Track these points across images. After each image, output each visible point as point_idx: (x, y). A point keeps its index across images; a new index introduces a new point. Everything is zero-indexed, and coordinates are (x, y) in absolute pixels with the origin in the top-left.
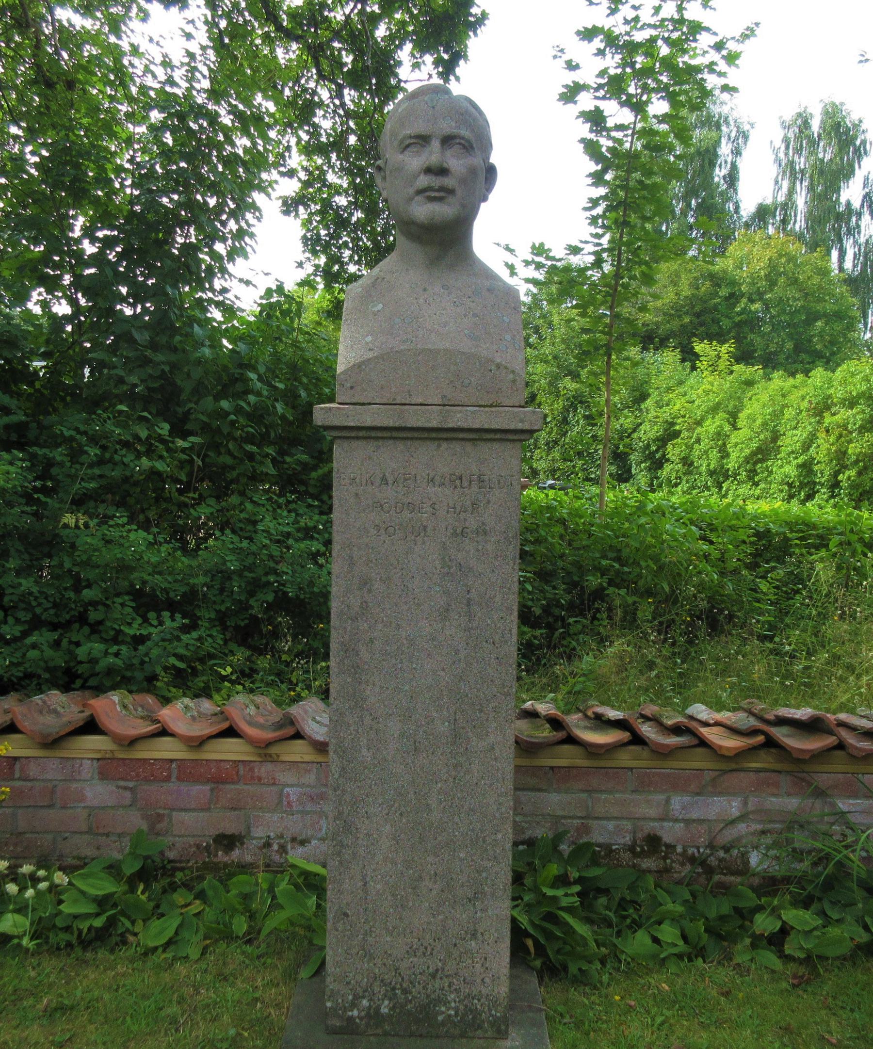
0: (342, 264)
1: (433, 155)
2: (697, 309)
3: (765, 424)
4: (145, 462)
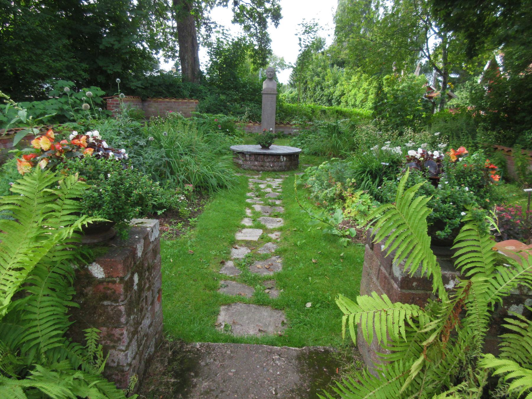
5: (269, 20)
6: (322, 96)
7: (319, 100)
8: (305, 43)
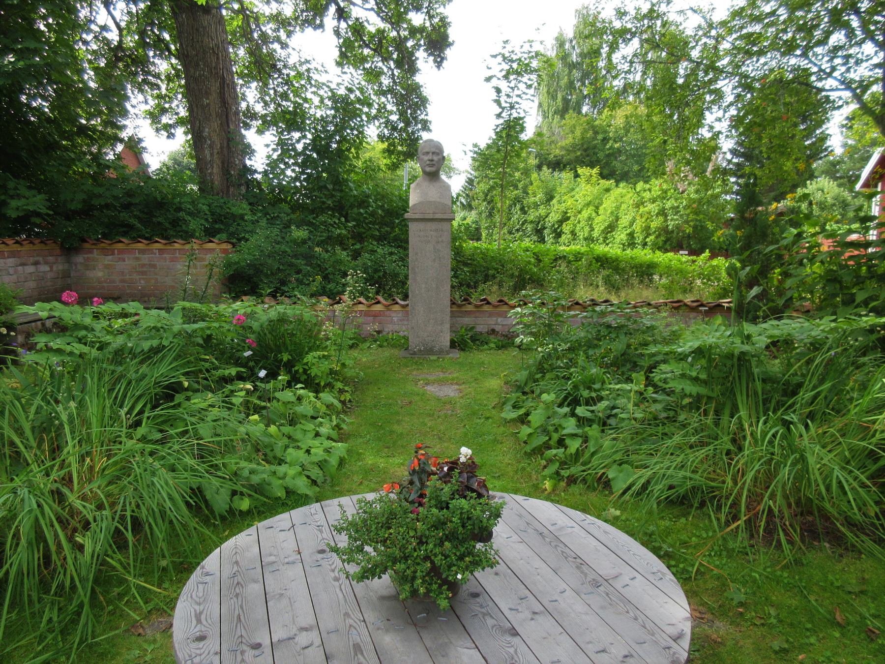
0: (395, 146)
1: (430, 157)
2: (585, 146)
3: (612, 213)
4: (339, 231)
5: (421, 54)
6: (523, 224)
7: (518, 230)
8: (509, 100)
